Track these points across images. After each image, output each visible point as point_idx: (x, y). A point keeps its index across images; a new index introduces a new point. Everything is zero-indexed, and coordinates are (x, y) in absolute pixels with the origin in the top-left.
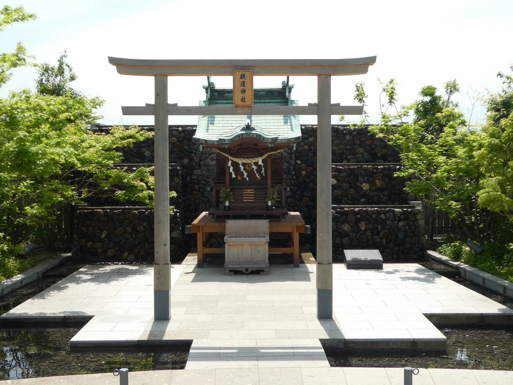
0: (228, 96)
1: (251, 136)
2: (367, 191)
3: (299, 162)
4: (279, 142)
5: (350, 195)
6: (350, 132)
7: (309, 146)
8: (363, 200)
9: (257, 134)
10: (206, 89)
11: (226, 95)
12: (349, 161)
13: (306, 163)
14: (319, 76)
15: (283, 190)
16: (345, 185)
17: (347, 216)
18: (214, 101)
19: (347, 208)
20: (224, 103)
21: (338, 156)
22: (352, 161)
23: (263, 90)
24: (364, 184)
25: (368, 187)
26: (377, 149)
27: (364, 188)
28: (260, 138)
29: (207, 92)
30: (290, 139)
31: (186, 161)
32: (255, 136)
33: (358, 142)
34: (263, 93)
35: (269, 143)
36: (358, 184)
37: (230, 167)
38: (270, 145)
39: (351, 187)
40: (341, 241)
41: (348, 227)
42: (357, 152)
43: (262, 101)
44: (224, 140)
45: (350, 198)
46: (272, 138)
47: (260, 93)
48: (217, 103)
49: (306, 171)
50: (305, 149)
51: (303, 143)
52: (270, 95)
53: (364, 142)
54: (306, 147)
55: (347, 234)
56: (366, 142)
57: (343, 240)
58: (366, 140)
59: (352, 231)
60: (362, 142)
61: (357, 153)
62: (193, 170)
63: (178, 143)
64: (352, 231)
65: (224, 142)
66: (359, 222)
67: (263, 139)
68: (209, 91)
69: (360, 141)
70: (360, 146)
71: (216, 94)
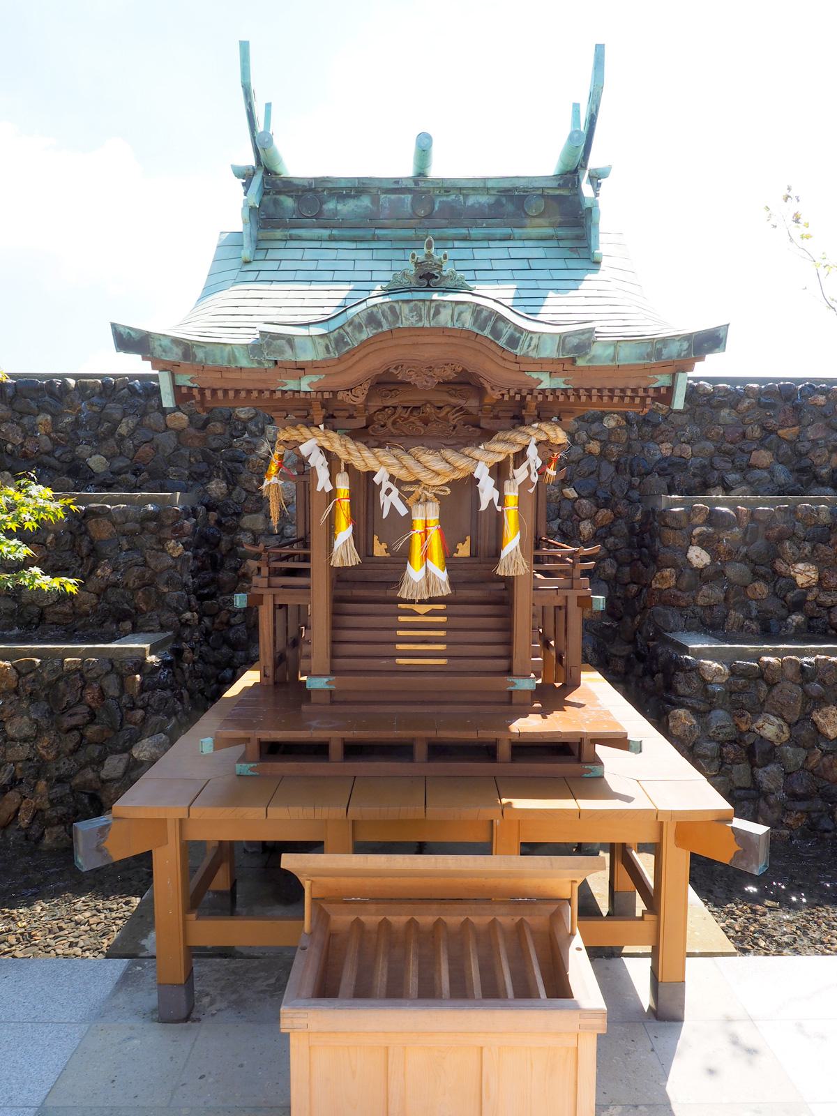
0: (336, 212)
1: (445, 318)
2: (809, 588)
3: (571, 493)
4: (600, 353)
5: (753, 604)
6: (748, 393)
7: (604, 444)
8: (797, 618)
9: (477, 310)
10: (246, 176)
11: (330, 205)
12: (728, 489)
13: (593, 495)
14: (373, 556)
15: (573, 603)
16: (736, 571)
17: (772, 685)
18: (279, 233)
19: (774, 653)
20: (320, 240)
21: (695, 475)
22: (740, 490)
23: (481, 186)
24: (800, 566)
25: (814, 576)
26: (818, 452)
27: (801, 580)
28: (496, 333)
29: (247, 186)
30: (665, 341)
31: (217, 487)
32: (468, 321)
33: (757, 433)
34: (484, 199)
35: (541, 364)
36: (781, 566)
37: (817, 660)
38: (546, 382)
39: (756, 576)
40: (753, 775)
41: (780, 727)
42: (752, 461)
43: (474, 232)
44: (290, 340)
45: (754, 613)
46: (563, 338)
47: (471, 200)
48: (292, 238)
49: (594, 522)
50: (591, 453)
51: (584, 436)
52: (510, 208)
53: (772, 432)
54: (595, 447)
55: (771, 752)
56: (780, 432)
57: (760, 773)
58: (782, 427)
59: (794, 741)
60: (768, 431)
61: (756, 467)
62: (238, 515)
63: (192, 431)
64: (794, 741)
65: (288, 356)
66: (819, 709)
67: (513, 342)
68: (257, 181)
69: (764, 428)
70: (762, 443)
71: (289, 202)
